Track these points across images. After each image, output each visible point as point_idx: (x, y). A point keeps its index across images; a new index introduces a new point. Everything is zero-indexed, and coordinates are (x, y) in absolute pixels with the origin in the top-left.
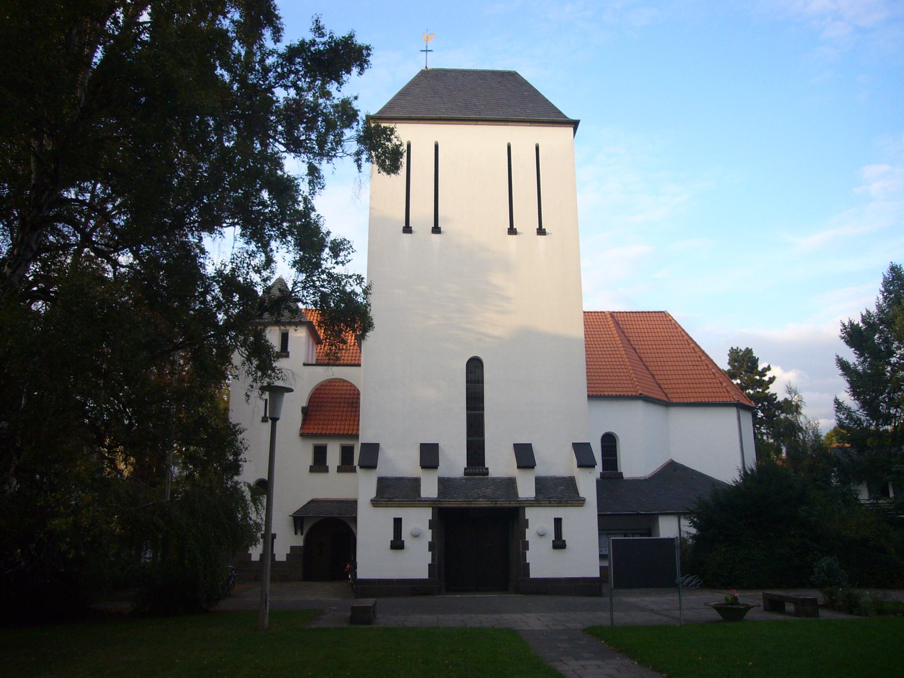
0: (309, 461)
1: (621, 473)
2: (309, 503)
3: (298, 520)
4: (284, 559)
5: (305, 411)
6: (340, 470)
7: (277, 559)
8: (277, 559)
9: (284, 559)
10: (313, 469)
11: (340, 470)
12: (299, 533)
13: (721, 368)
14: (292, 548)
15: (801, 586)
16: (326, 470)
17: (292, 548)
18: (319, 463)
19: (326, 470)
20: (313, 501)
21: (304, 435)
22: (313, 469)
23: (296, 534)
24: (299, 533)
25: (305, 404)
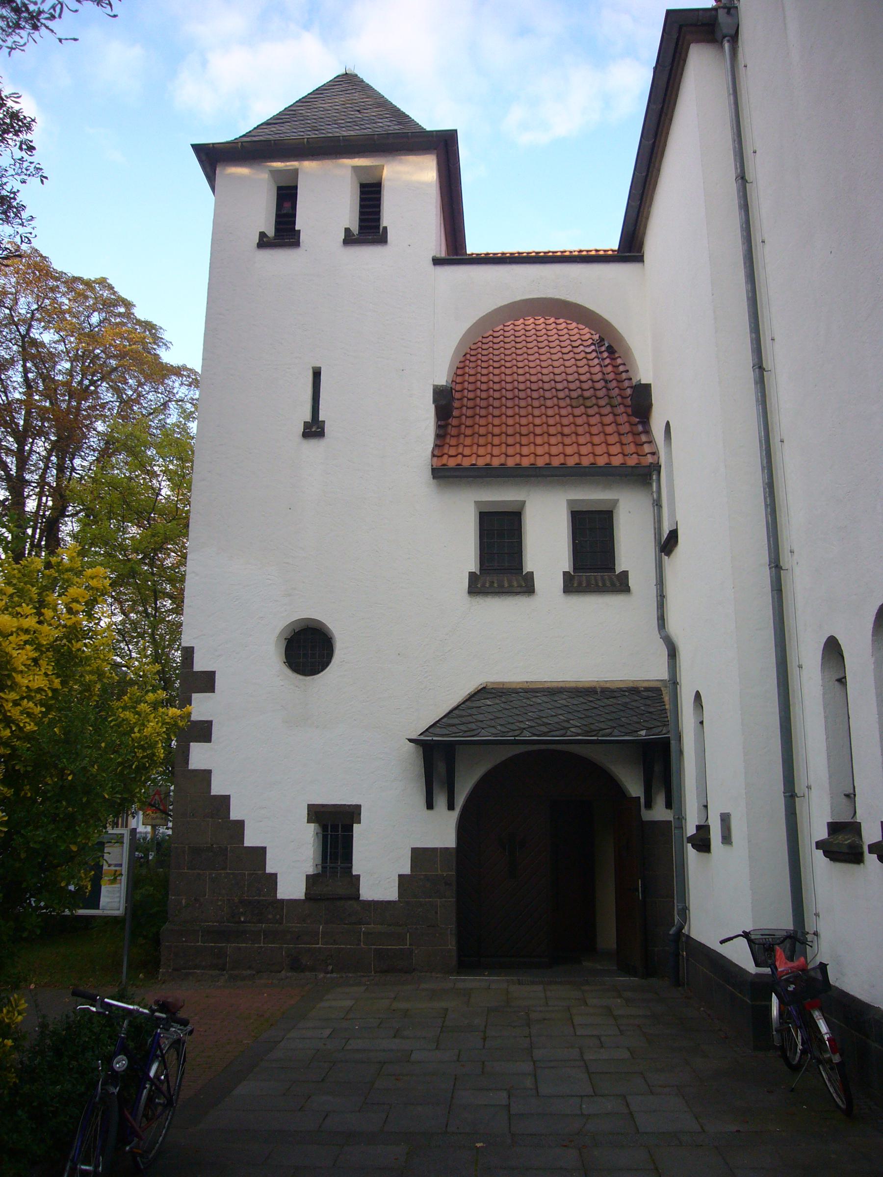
0: (466, 557)
1: (240, 825)
2: (471, 697)
3: (437, 756)
4: (392, 894)
5: (445, 402)
6: (573, 584)
7: (368, 892)
8: (368, 892)
9: (392, 894)
10: (479, 586)
11: (573, 584)
12: (441, 801)
13: (360, 864)
14: (419, 855)
15: (539, 751)
16: (526, 586)
17: (419, 855)
18: (500, 563)
19: (526, 586)
20: (483, 692)
21: (444, 474)
22: (479, 586)
23: (430, 805)
24: (441, 801)
25: (442, 379)
